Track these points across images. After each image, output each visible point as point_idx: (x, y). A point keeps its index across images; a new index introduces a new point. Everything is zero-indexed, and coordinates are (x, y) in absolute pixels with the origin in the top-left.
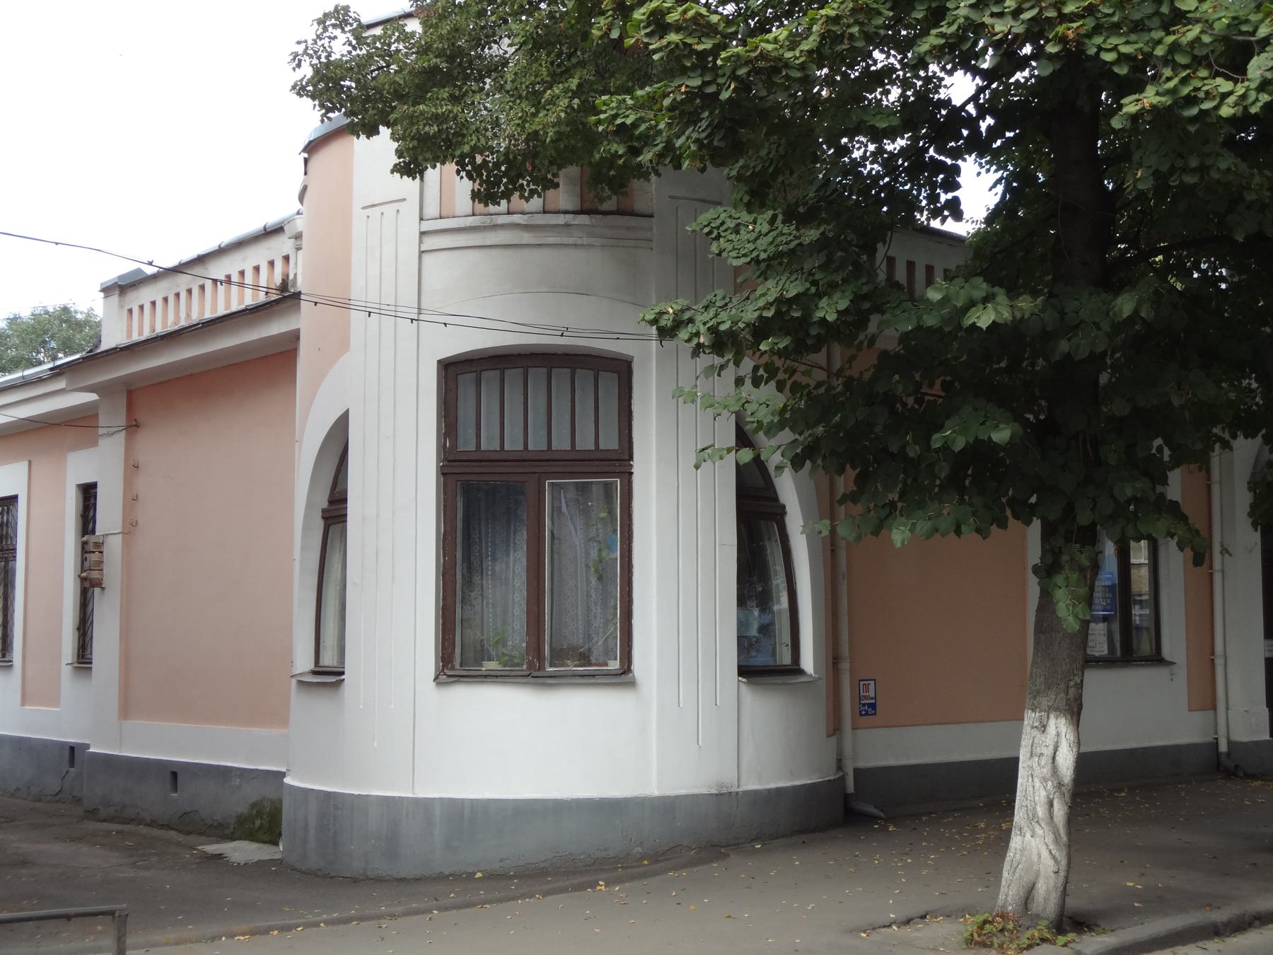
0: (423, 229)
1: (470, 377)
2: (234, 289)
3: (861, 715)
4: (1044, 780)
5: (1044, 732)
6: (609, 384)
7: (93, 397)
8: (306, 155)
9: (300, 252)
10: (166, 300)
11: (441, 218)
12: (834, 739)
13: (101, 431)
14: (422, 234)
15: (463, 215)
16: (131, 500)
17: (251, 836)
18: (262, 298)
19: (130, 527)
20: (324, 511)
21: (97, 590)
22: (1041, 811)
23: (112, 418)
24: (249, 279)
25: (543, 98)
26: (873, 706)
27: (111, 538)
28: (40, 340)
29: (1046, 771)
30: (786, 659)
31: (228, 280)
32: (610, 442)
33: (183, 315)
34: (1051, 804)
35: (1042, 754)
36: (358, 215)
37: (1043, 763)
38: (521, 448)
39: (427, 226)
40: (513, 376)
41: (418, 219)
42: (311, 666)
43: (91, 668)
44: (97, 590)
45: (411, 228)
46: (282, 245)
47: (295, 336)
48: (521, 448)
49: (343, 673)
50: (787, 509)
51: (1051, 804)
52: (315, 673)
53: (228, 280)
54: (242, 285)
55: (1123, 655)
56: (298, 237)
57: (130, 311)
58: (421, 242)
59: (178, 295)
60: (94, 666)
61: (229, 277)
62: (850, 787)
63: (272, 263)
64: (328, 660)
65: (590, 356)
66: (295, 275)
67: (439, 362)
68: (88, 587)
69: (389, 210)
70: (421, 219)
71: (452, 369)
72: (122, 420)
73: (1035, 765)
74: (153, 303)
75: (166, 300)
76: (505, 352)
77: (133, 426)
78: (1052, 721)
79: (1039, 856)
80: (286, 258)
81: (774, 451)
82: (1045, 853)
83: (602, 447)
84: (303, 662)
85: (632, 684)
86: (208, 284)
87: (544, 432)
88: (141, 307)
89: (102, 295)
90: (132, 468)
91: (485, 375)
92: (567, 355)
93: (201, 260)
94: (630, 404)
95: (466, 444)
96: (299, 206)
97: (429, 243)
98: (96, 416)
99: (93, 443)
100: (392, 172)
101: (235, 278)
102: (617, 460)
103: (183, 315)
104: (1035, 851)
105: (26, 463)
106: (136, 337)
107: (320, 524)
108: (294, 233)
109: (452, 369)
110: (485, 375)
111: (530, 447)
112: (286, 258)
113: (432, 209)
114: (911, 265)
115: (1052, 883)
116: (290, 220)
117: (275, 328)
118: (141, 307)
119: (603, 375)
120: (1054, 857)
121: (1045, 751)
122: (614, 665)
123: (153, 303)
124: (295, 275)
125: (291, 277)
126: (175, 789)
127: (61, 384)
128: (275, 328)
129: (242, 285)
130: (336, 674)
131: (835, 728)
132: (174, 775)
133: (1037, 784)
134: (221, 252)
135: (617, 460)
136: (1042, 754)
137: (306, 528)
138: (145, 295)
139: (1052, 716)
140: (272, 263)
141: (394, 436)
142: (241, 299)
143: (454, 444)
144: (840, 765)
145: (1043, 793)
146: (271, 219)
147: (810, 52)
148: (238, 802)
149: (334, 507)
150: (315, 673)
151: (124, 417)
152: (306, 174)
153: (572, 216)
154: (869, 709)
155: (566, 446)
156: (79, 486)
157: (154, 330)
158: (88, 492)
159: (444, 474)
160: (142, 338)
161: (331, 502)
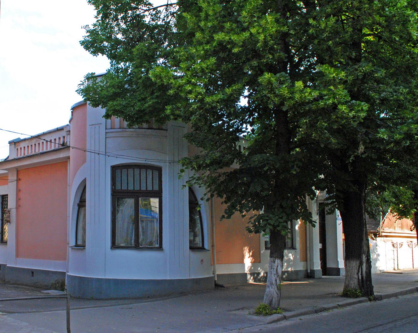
0: (107, 132)
1: (126, 170)
4: (275, 274)
5: (274, 263)
6: (156, 173)
8: (72, 110)
10: (28, 146)
11: (111, 129)
13: (9, 181)
16: (18, 199)
17: (56, 289)
18: (57, 147)
19: (18, 207)
20: (78, 204)
22: (274, 282)
24: (57, 141)
25: (249, 96)
27: (12, 209)
29: (275, 272)
31: (51, 141)
32: (156, 188)
34: (276, 280)
35: (274, 268)
37: (274, 270)
38: (145, 189)
39: (107, 131)
40: (131, 171)
41: (105, 129)
42: (74, 244)
45: (103, 131)
48: (145, 189)
49: (85, 246)
51: (276, 280)
52: (76, 246)
53: (51, 141)
55: (135, 245)
57: (17, 149)
58: (106, 135)
59: (32, 145)
63: (60, 138)
64: (80, 243)
66: (67, 142)
69: (97, 127)
70: (106, 129)
71: (114, 168)
73: (272, 271)
74: (24, 147)
75: (28, 146)
78: (276, 260)
79: (273, 293)
80: (64, 137)
81: (201, 191)
82: (275, 293)
83: (148, 189)
84: (72, 243)
85: (162, 250)
86: (45, 142)
88: (21, 148)
89: (9, 144)
90: (18, 191)
91: (123, 170)
94: (161, 179)
95: (118, 187)
96: (69, 123)
97: (107, 131)
98: (7, 177)
100: (103, 117)
103: (30, 151)
104: (272, 292)
106: (19, 156)
107: (77, 208)
109: (114, 168)
111: (123, 188)
112: (64, 137)
113: (109, 126)
114: (240, 146)
115: (276, 299)
117: (62, 155)
118: (21, 148)
120: (277, 293)
121: (275, 267)
122: (157, 246)
123: (24, 147)
124: (67, 142)
125: (65, 142)
126: (33, 276)
128: (62, 155)
130: (83, 246)
132: (33, 272)
133: (273, 276)
136: (274, 268)
137: (73, 208)
138: (22, 145)
139: (276, 259)
140: (60, 138)
141: (99, 185)
143: (115, 187)
145: (274, 278)
147: (235, 90)
148: (52, 280)
149: (81, 203)
150: (76, 246)
151: (16, 177)
153: (146, 130)
155: (151, 189)
157: (25, 155)
159: (112, 195)
160: (21, 157)
161: (80, 202)
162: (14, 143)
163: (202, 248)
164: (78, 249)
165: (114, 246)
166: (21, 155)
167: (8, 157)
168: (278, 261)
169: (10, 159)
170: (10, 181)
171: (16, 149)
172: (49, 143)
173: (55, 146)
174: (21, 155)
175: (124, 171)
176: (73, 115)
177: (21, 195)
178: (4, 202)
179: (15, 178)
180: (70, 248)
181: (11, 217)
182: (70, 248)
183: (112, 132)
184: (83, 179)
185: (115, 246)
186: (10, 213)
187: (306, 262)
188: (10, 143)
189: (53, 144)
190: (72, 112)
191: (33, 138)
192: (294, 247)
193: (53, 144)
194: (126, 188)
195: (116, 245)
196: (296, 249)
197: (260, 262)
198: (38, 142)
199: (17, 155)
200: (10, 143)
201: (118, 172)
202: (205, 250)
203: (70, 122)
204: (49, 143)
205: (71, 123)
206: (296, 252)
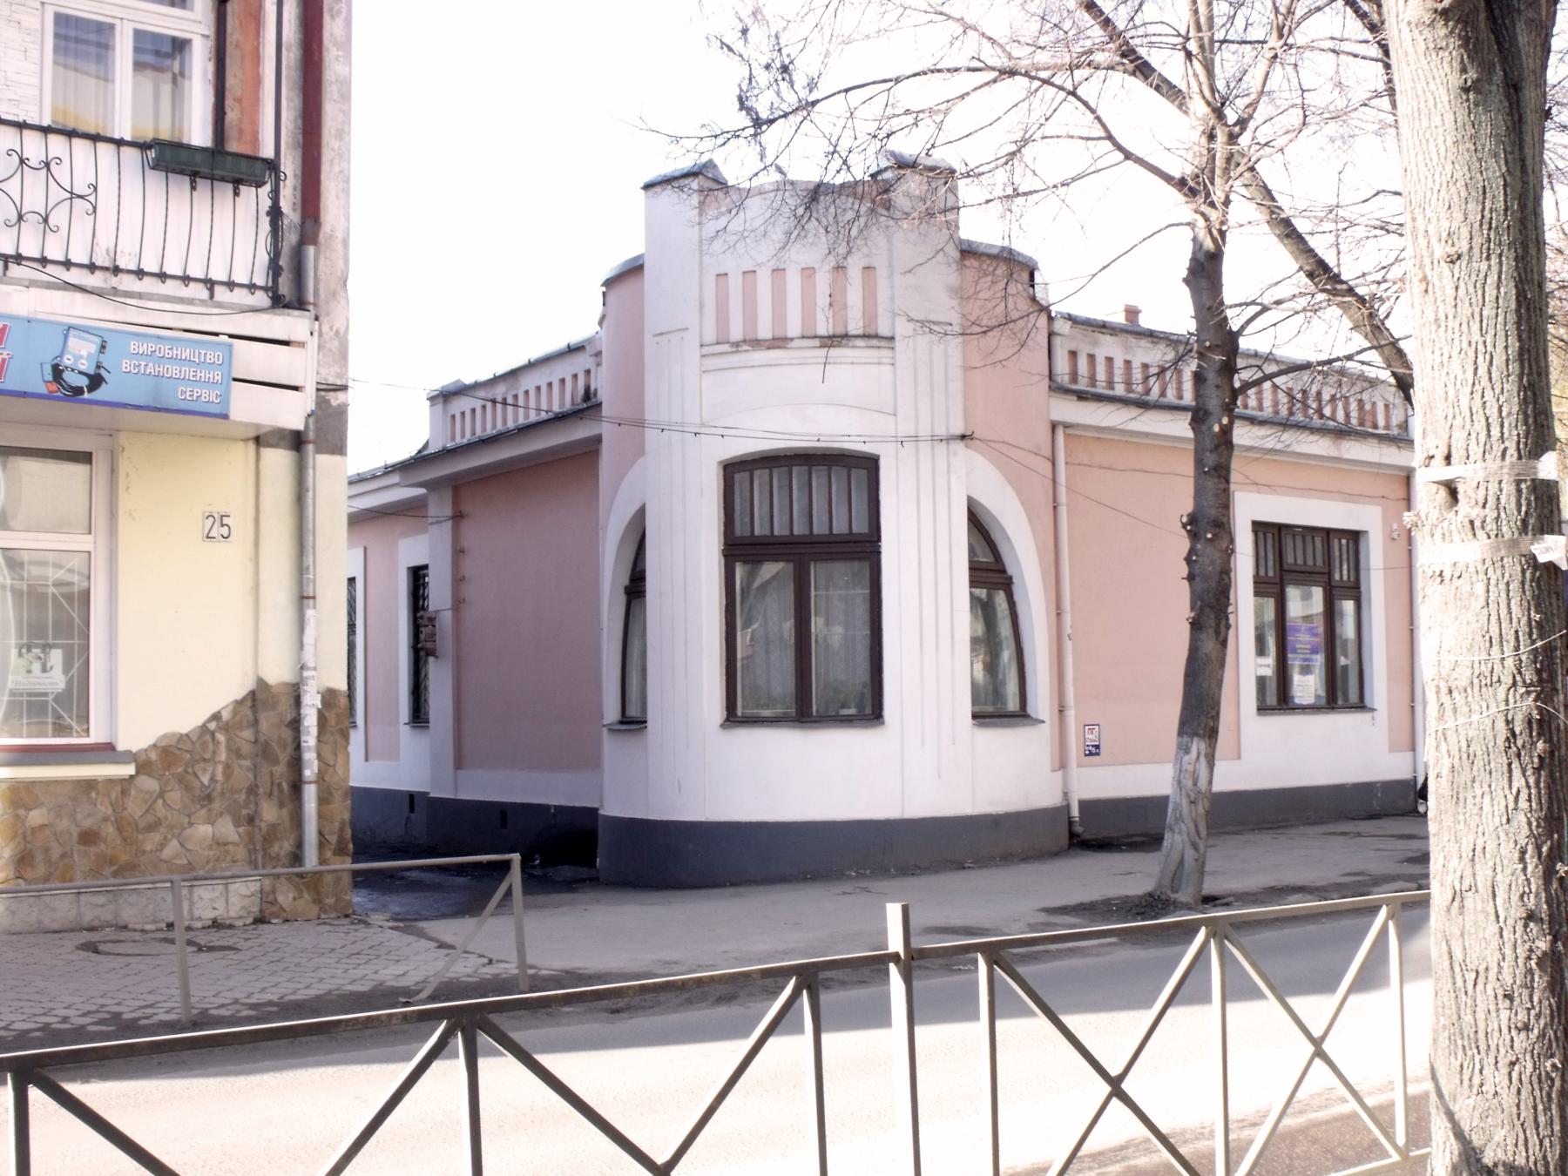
2: (510, 409)
3: (1086, 755)
6: (859, 475)
7: (422, 491)
8: (604, 289)
9: (599, 368)
11: (718, 343)
12: (1059, 774)
14: (703, 356)
15: (250, 567)
16: (458, 580)
19: (458, 603)
20: (626, 588)
21: (431, 659)
23: (441, 507)
24: (521, 402)
26: (1097, 747)
28: (1433, 128)
30: (1012, 704)
32: (860, 526)
33: (489, 427)
36: (649, 340)
39: (706, 350)
43: (428, 727)
44: (431, 659)
46: (580, 363)
47: (598, 439)
50: (1014, 580)
52: (622, 723)
53: (504, 403)
54: (516, 406)
56: (598, 354)
57: (453, 417)
60: (431, 725)
61: (505, 399)
62: (1075, 812)
64: (633, 712)
65: (844, 455)
67: (720, 462)
68: (420, 654)
72: (448, 511)
76: (773, 454)
77: (458, 517)
80: (588, 372)
84: (612, 712)
86: (489, 405)
87: (806, 520)
89: (428, 402)
90: (458, 552)
92: (825, 455)
93: (513, 374)
95: (740, 530)
97: (706, 350)
99: (425, 531)
101: (510, 400)
102: (868, 542)
103: (489, 427)
105: (362, 549)
106: (459, 441)
108: (595, 351)
110: (757, 473)
112: (588, 372)
116: (590, 340)
117: (579, 432)
119: (854, 472)
127: (395, 478)
128: (579, 432)
129: (516, 406)
131: (1063, 765)
134: (531, 366)
135: (868, 542)
140: (575, 376)
142: (516, 419)
144: (1066, 794)
146: (575, 338)
150: (622, 723)
152: (604, 305)
154: (1094, 751)
156: (409, 568)
158: (418, 576)
160: (465, 441)
162: (445, 397)
163: (1021, 715)
164: (626, 730)
165: (733, 718)
166: (463, 436)
167: (427, 443)
168: (1198, 746)
169: (431, 450)
170: (434, 520)
171: (449, 419)
172: (499, 406)
173: (527, 416)
174: (463, 436)
175: (760, 476)
176: (608, 303)
177: (468, 566)
178: (421, 591)
179: (448, 511)
180: (605, 730)
181: (437, 639)
182: (605, 730)
183: (721, 354)
184: (636, 507)
185: (736, 716)
186: (434, 626)
187: (1411, 753)
188: (432, 399)
189: (521, 411)
190: (604, 294)
191: (496, 380)
192: (1368, 702)
193: (521, 411)
194: (787, 532)
195: (739, 714)
196: (1373, 710)
197: (1239, 757)
198: (514, 393)
199: (453, 439)
200: (432, 399)
201: (740, 478)
202: (1030, 722)
203: (600, 323)
204: (499, 406)
205: (604, 326)
206: (1373, 719)
